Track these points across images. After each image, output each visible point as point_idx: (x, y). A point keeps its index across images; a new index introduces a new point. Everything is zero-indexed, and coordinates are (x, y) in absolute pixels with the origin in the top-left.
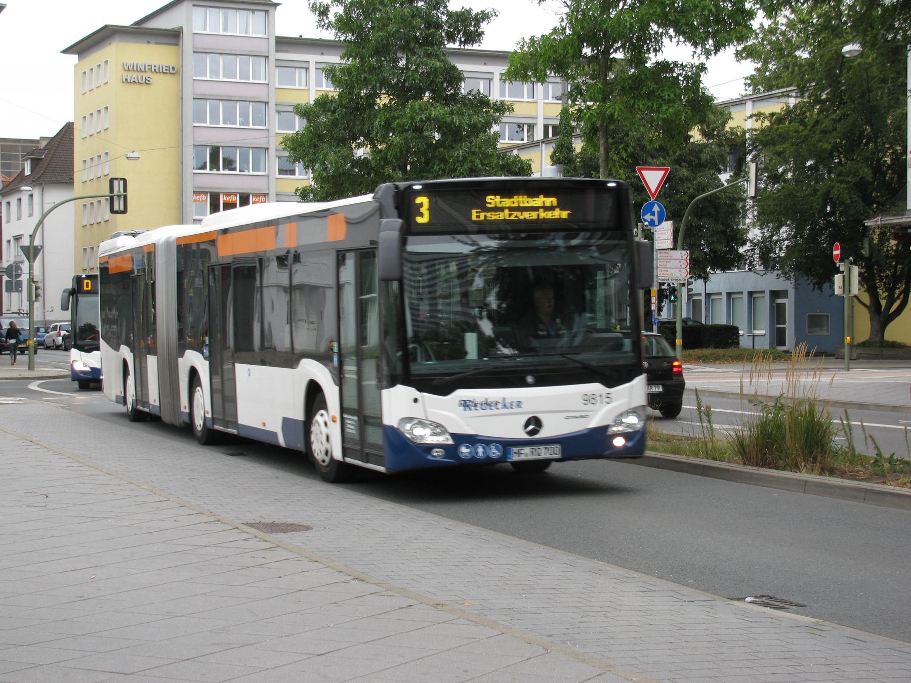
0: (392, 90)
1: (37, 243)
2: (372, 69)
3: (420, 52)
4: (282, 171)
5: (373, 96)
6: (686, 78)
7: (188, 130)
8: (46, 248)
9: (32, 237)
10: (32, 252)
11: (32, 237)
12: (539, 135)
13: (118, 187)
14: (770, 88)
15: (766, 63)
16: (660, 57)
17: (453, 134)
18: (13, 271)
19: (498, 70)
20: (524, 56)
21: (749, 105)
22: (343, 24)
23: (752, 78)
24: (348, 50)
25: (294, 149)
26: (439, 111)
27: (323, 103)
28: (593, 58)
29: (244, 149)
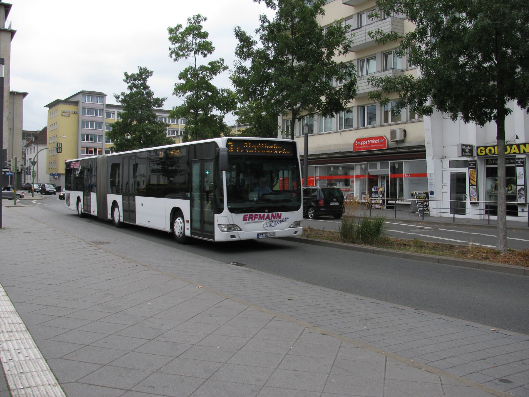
1: (35, 161)
5: (131, 122)
6: (219, 119)
7: (80, 130)
9: (34, 159)
10: (34, 163)
11: (34, 159)
12: (179, 134)
13: (59, 145)
14: (242, 123)
15: (241, 117)
16: (212, 113)
17: (154, 133)
18: (29, 168)
19: (167, 115)
20: (174, 111)
21: (237, 128)
22: (123, 101)
23: (238, 120)
24: (125, 108)
25: (109, 136)
27: (117, 123)
28: (194, 113)
29: (96, 136)
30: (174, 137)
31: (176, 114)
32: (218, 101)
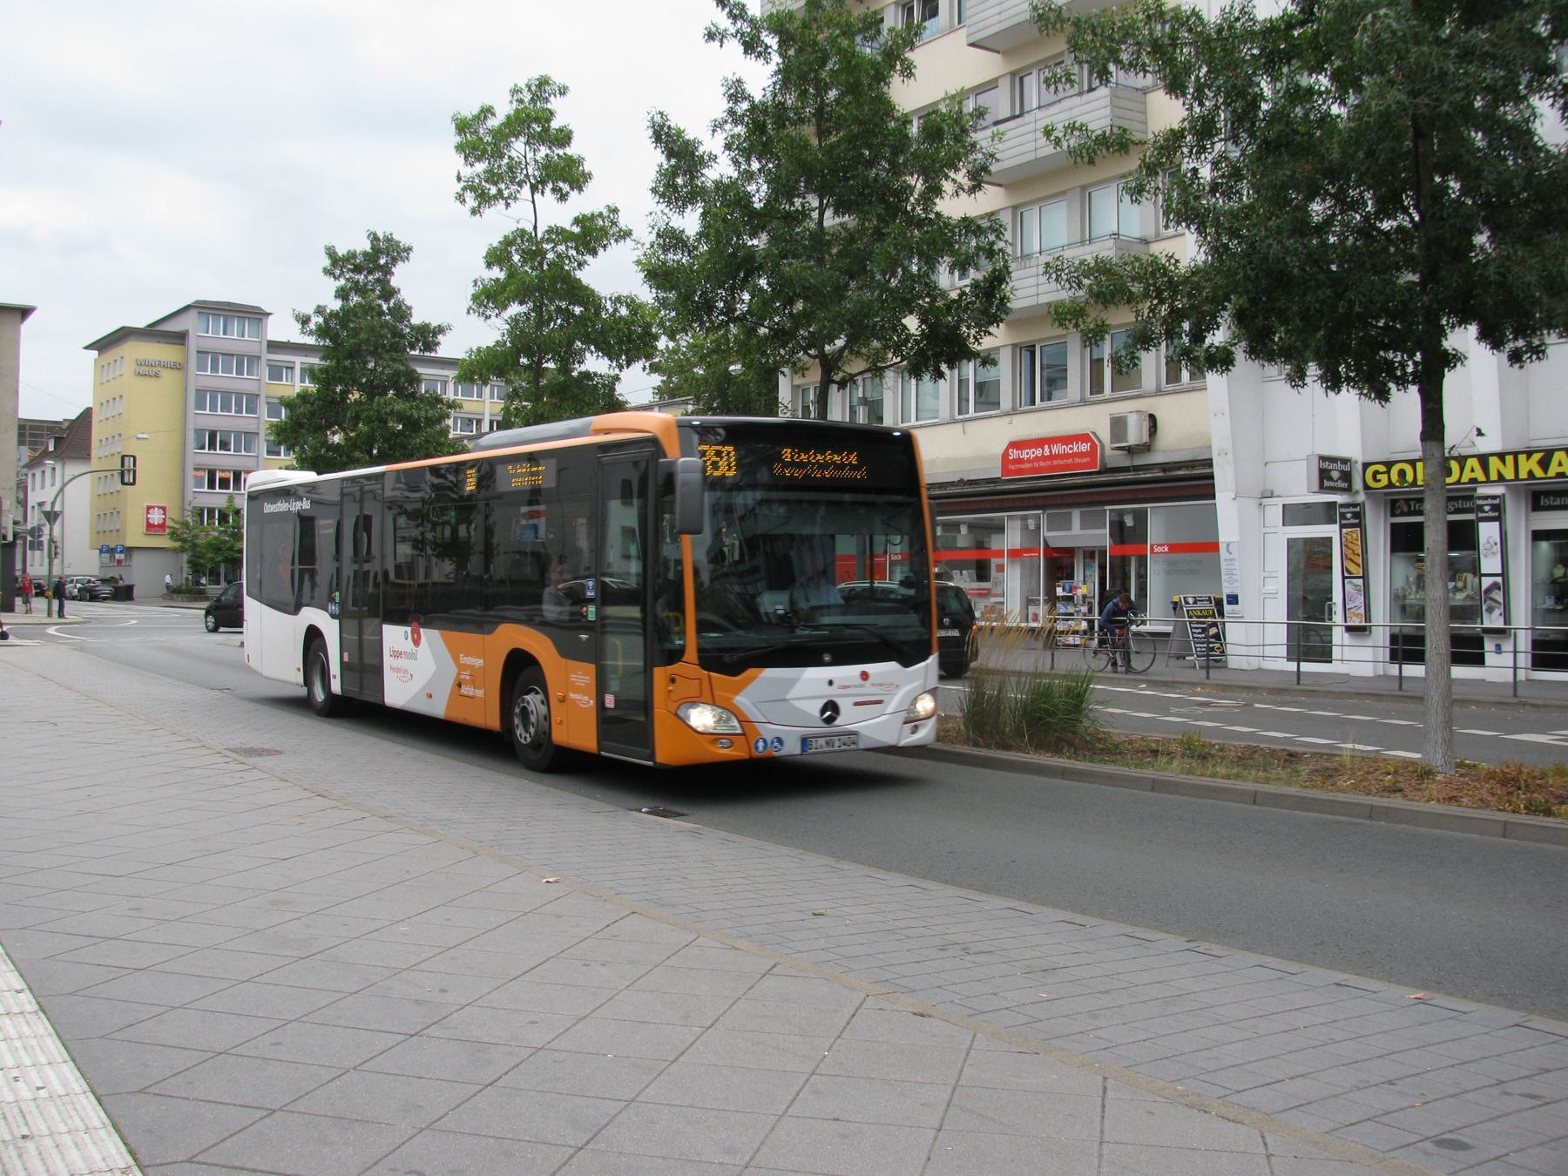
0: (361, 388)
1: (57, 508)
2: (345, 368)
3: (386, 356)
4: (269, 453)
5: (345, 393)
6: (604, 385)
8: (67, 512)
9: (53, 504)
10: (52, 516)
11: (53, 504)
13: (129, 463)
15: (670, 377)
16: (583, 368)
17: (413, 425)
18: (36, 532)
19: (451, 374)
20: (472, 363)
22: (322, 332)
23: (659, 388)
24: (326, 353)
25: (278, 435)
26: (400, 406)
27: (304, 397)
29: (238, 434)
30: (470, 438)
31: (479, 369)
32: (603, 332)
